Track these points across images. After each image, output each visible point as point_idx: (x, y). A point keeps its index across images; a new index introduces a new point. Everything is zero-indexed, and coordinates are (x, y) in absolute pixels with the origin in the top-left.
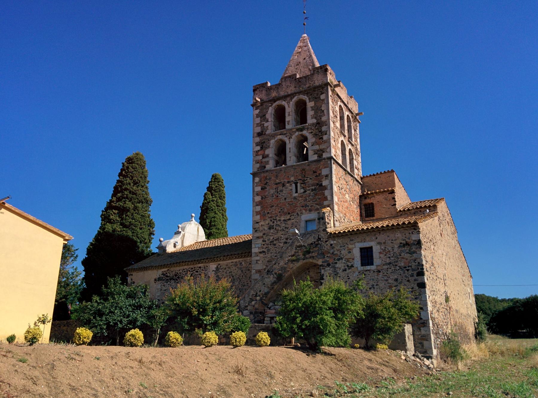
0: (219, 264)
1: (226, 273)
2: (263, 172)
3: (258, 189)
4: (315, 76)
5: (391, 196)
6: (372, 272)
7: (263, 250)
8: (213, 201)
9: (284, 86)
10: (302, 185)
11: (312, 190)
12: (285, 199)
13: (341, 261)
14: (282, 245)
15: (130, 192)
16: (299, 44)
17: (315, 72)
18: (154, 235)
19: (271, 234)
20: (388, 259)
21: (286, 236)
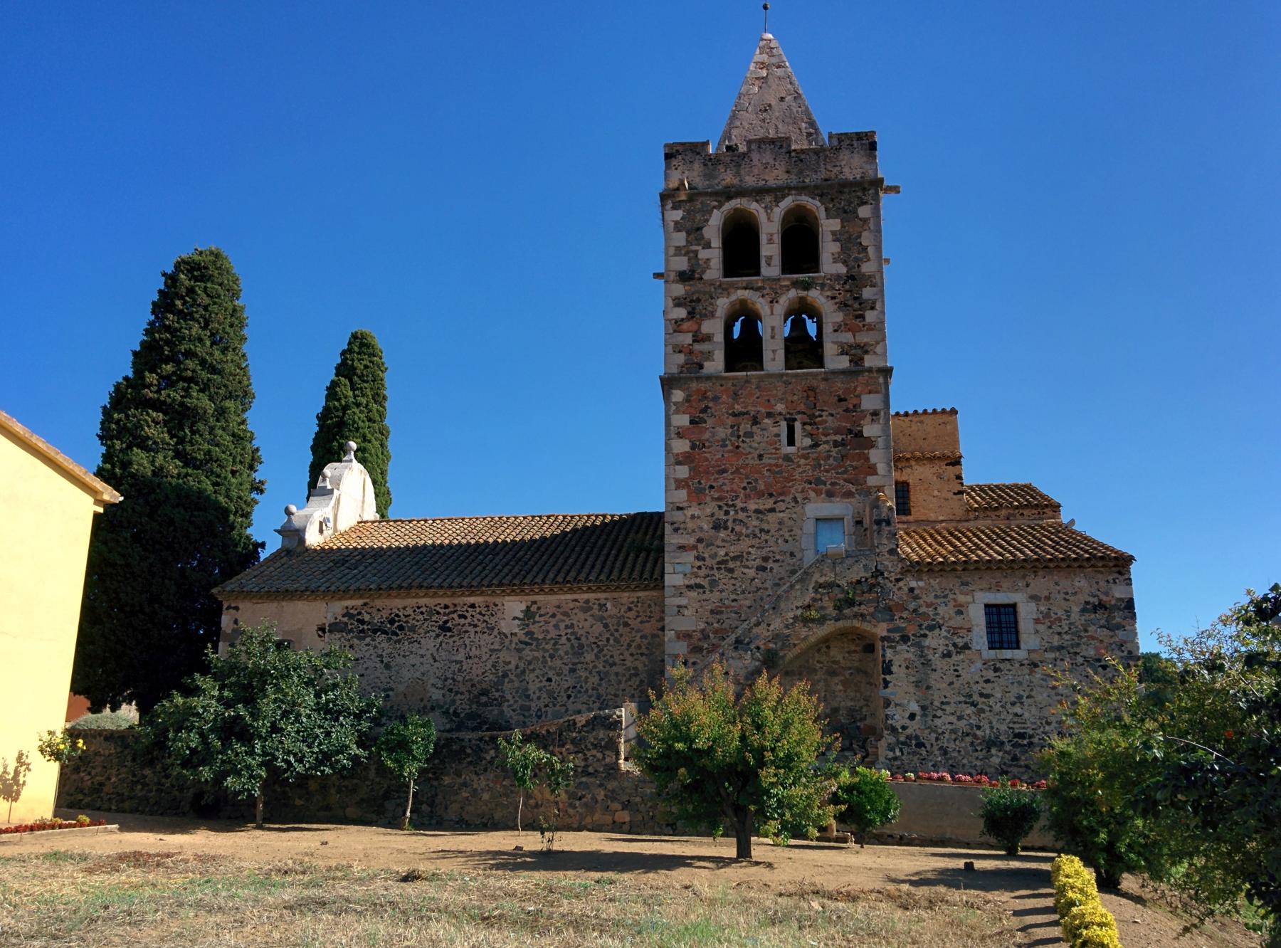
0: (534, 602)
1: (556, 626)
2: (698, 378)
3: (682, 420)
4: (845, 156)
5: (951, 470)
6: (1017, 665)
7: (698, 581)
8: (358, 405)
9: (755, 162)
10: (808, 428)
11: (836, 444)
12: (760, 457)
13: (937, 631)
14: (751, 573)
15: (203, 362)
16: (758, 57)
17: (844, 144)
18: (262, 492)
19: (719, 543)
20: (1057, 637)
21: (764, 553)
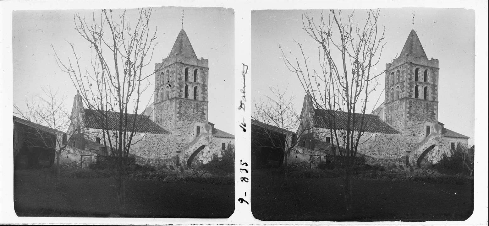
7: (180, 134)
